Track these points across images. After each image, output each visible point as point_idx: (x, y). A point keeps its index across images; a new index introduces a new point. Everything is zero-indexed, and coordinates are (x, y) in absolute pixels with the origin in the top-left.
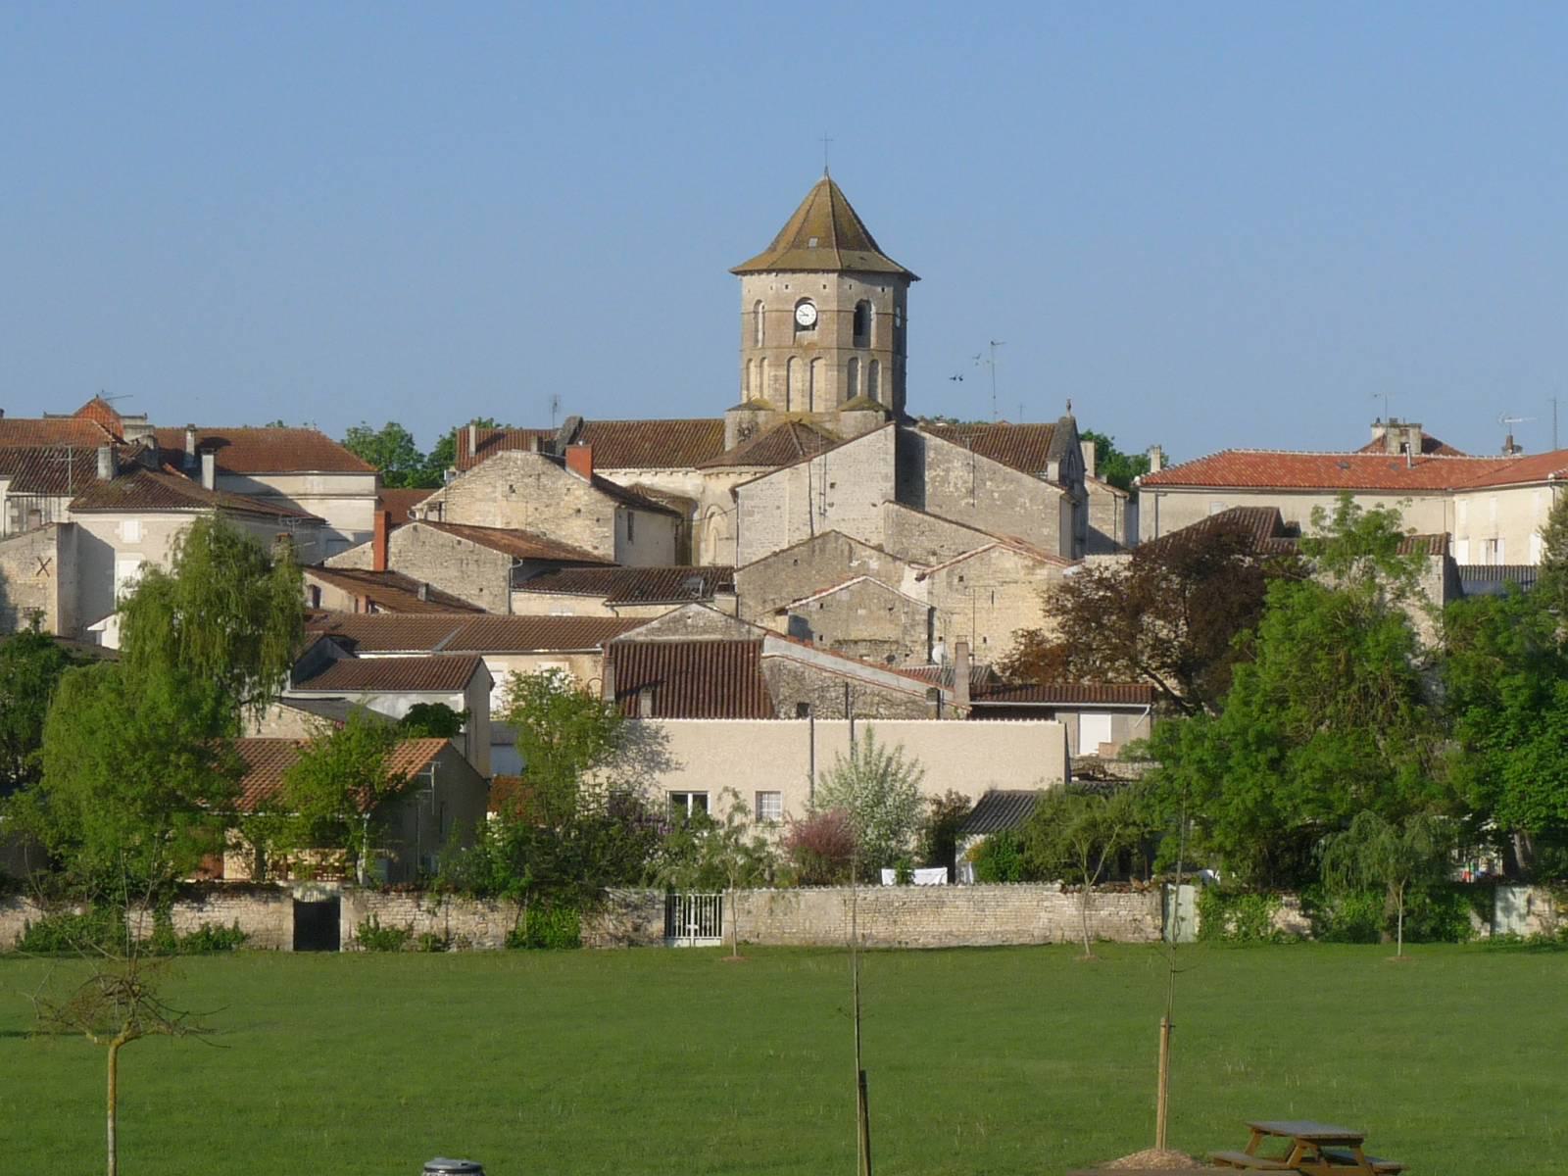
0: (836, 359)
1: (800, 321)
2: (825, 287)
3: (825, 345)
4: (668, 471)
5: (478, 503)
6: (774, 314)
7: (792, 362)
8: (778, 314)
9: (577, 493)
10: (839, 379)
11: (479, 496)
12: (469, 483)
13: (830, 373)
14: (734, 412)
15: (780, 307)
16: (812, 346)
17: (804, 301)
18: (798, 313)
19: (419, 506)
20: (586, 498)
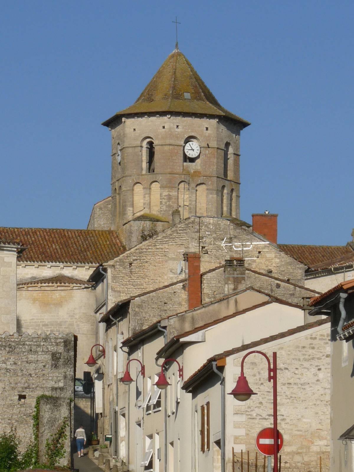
0: (215, 185)
1: (187, 154)
2: (207, 129)
3: (208, 173)
4: (36, 264)
5: (170, 262)
6: (166, 148)
7: (183, 183)
8: (171, 147)
9: (268, 255)
10: (217, 200)
11: (171, 255)
12: (162, 243)
13: (211, 196)
14: (137, 222)
15: (172, 142)
16: (197, 173)
17: (188, 140)
18: (186, 148)
19: (111, 263)
20: (278, 260)
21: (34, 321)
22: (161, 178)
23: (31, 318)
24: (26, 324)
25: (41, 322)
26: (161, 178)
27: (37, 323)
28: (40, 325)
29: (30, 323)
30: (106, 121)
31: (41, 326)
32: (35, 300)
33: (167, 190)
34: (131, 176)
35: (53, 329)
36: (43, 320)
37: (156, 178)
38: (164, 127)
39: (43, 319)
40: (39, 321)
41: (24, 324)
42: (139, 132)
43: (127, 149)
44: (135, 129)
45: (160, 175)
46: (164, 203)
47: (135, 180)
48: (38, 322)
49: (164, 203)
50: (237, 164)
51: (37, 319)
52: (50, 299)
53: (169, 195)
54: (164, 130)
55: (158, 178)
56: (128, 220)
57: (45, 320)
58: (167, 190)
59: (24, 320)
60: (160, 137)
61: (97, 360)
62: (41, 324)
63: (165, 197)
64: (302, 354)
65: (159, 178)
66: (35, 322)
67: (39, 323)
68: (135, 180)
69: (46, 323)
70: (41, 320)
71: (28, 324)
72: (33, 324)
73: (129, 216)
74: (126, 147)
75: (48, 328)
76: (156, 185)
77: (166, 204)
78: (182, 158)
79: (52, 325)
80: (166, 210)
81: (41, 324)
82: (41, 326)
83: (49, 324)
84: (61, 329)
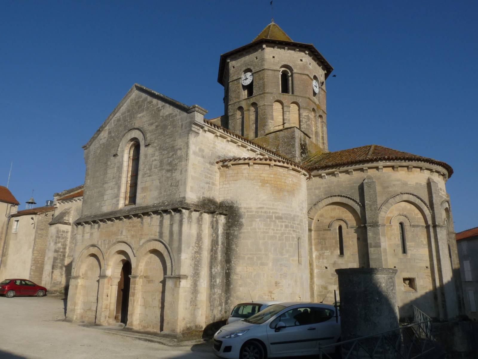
21: (263, 210)
22: (300, 100)
23: (259, 206)
24: (249, 213)
25: (273, 213)
26: (300, 100)
27: (268, 214)
28: (272, 216)
29: (257, 212)
30: (230, 52)
31: (274, 219)
32: (264, 182)
33: (307, 112)
34: (272, 93)
35: (287, 224)
36: (275, 211)
37: (296, 100)
38: (301, 60)
39: (276, 209)
40: (271, 212)
41: (246, 214)
42: (278, 59)
43: (267, 71)
44: (274, 57)
45: (300, 98)
46: (304, 122)
47: (276, 97)
48: (270, 213)
49: (304, 122)
50: (73, 190)
51: (268, 208)
52: (283, 184)
53: (308, 116)
54: (301, 62)
55: (298, 100)
56: (270, 131)
57: (278, 211)
58: (307, 112)
59: (245, 208)
60: (298, 67)
61: (369, 265)
62: (274, 216)
63: (306, 117)
64: (149, 278)
65: (299, 100)
66: (265, 212)
67: (271, 214)
68: (276, 97)
69: (280, 215)
70: (274, 211)
71: (254, 213)
72: (263, 214)
73: (271, 127)
74: (266, 69)
75: (283, 222)
76: (293, 106)
77: (307, 122)
78: (312, 94)
79: (287, 218)
80: (307, 128)
81: (274, 216)
82: (274, 219)
83: (283, 216)
84: (294, 225)
